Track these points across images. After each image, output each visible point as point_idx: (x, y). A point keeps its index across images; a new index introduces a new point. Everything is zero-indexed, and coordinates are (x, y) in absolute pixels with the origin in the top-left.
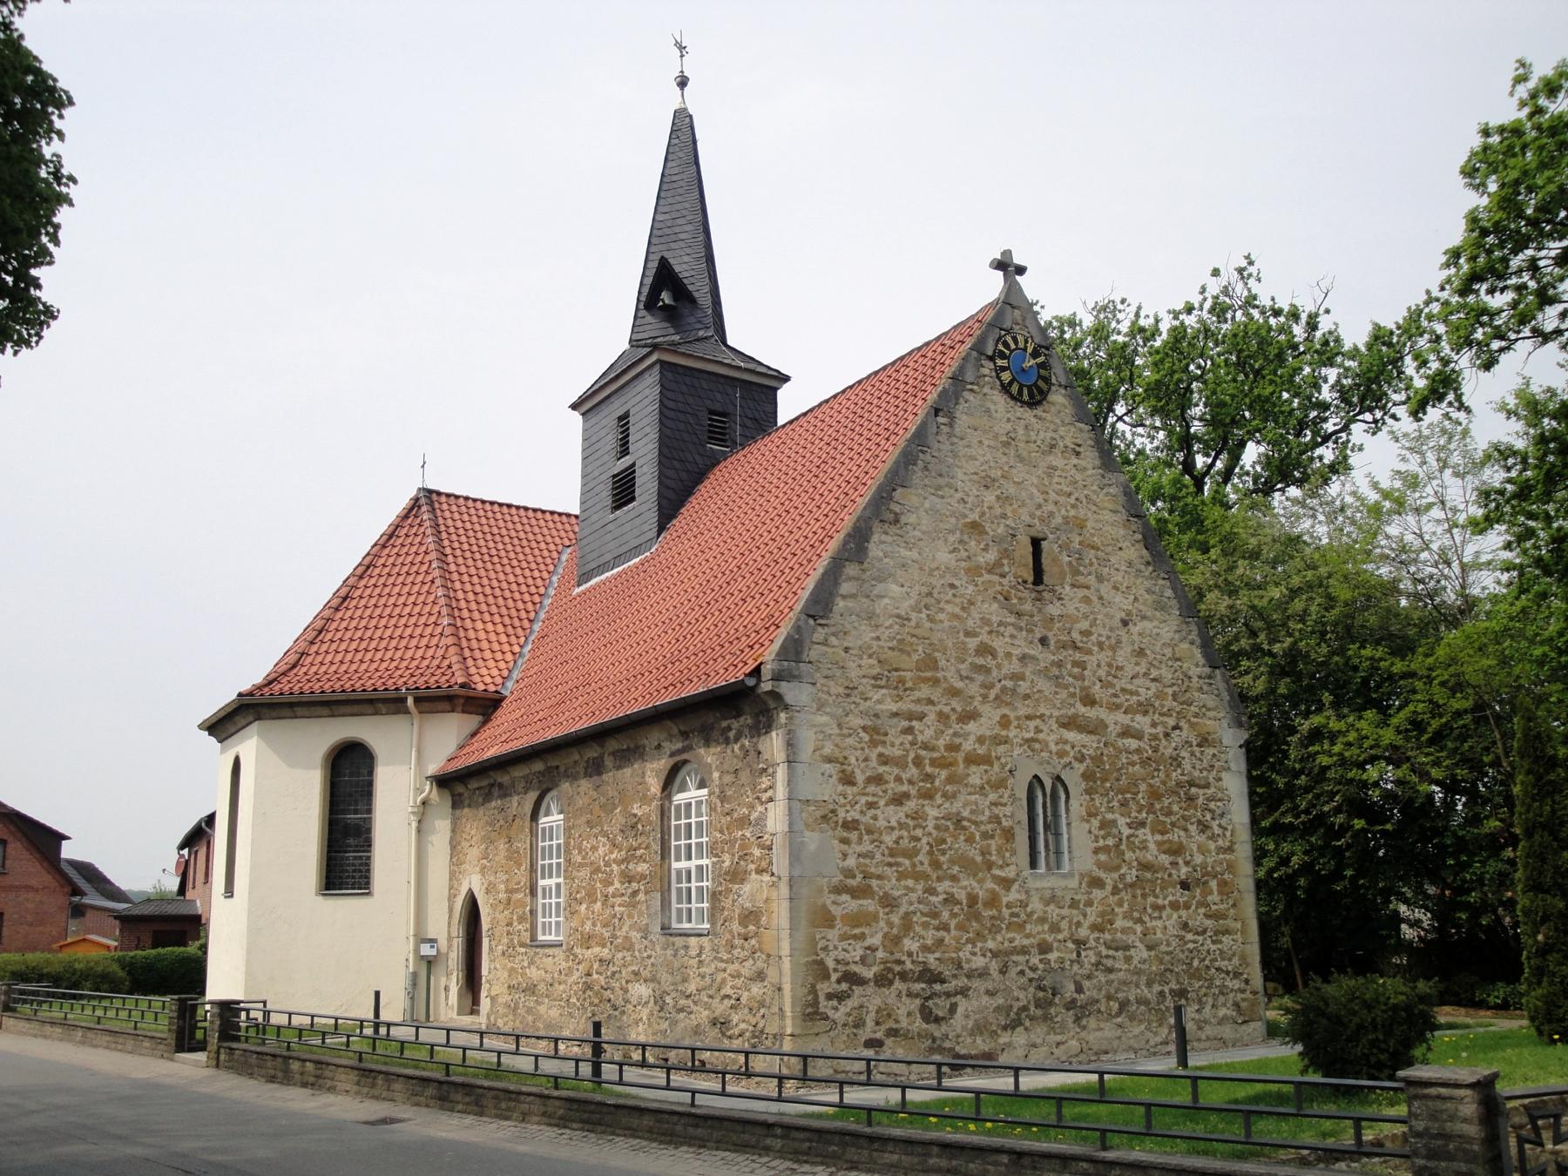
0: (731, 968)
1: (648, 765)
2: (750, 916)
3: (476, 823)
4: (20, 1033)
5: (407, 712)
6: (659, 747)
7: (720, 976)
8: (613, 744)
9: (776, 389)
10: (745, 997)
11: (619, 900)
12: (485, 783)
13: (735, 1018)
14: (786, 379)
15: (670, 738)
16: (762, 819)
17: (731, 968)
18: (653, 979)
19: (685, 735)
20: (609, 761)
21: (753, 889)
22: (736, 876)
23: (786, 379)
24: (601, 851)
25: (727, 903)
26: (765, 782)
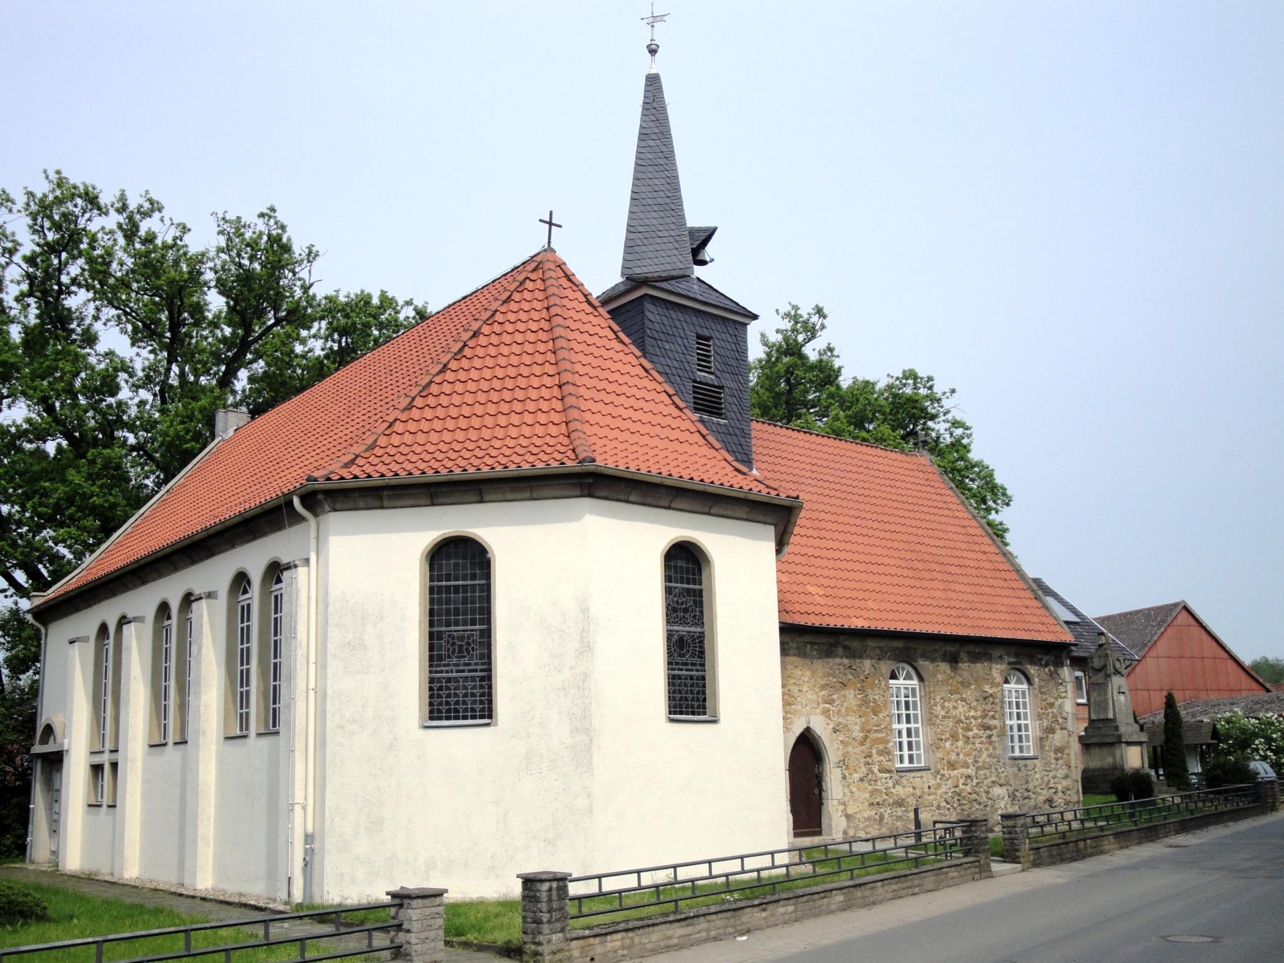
0: (1051, 774)
1: (994, 665)
2: (1059, 750)
3: (811, 674)
4: (200, 649)
5: (302, 519)
6: (1001, 657)
7: (1046, 779)
8: (970, 648)
9: (745, 325)
10: (1060, 788)
11: (978, 741)
12: (832, 641)
13: (1056, 798)
14: (755, 317)
15: (1008, 655)
16: (1061, 706)
17: (1051, 774)
18: (1008, 784)
19: (1016, 655)
20: (963, 655)
21: (1058, 738)
22: (1050, 730)
23: (755, 317)
24: (961, 709)
25: (1047, 743)
26: (1062, 689)
